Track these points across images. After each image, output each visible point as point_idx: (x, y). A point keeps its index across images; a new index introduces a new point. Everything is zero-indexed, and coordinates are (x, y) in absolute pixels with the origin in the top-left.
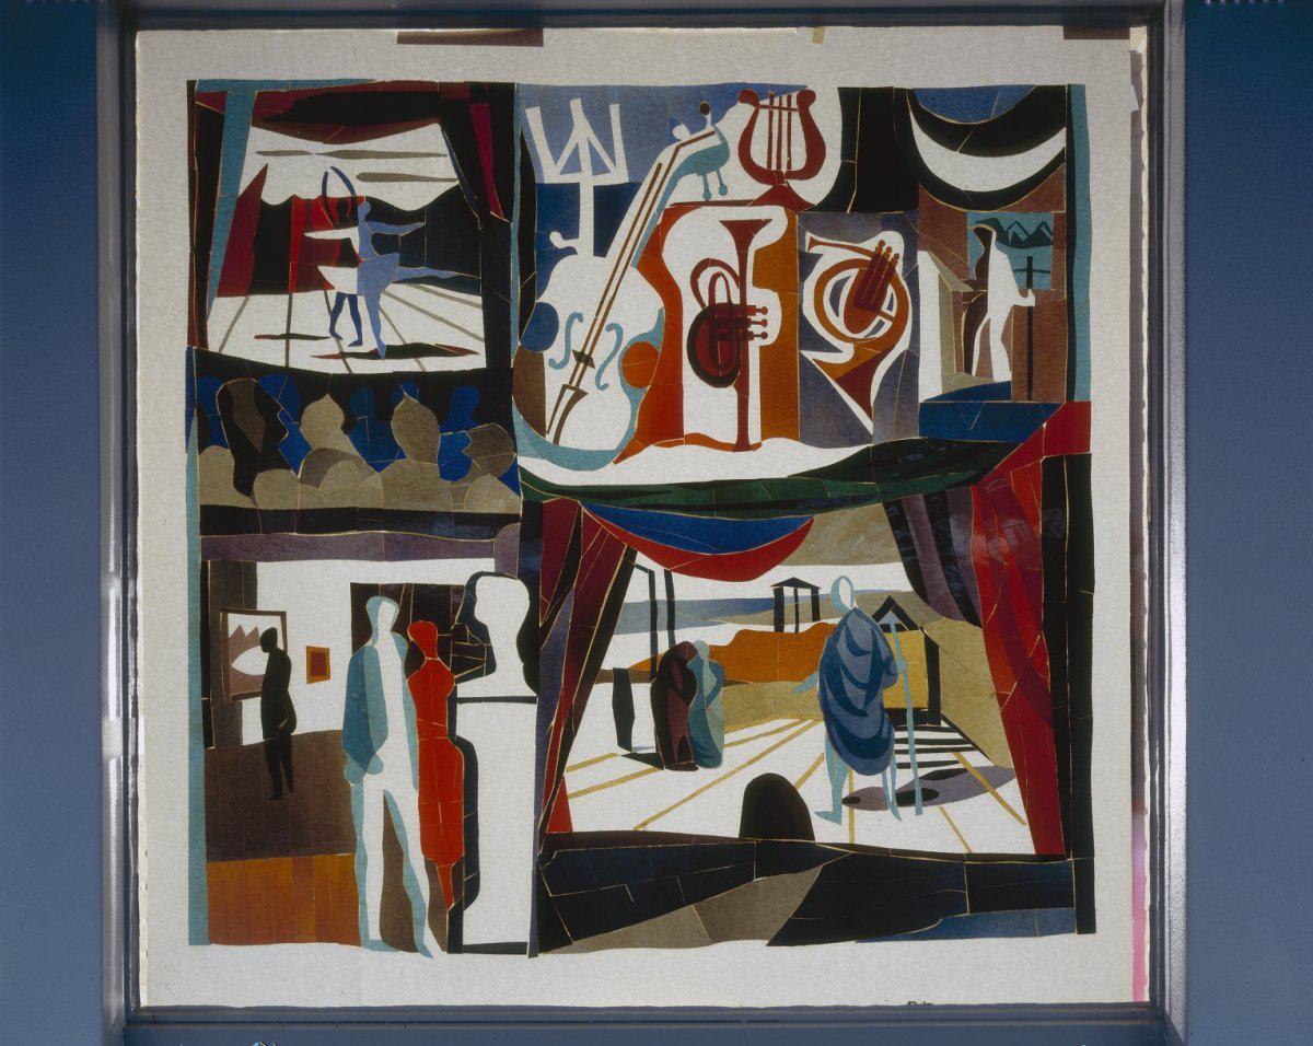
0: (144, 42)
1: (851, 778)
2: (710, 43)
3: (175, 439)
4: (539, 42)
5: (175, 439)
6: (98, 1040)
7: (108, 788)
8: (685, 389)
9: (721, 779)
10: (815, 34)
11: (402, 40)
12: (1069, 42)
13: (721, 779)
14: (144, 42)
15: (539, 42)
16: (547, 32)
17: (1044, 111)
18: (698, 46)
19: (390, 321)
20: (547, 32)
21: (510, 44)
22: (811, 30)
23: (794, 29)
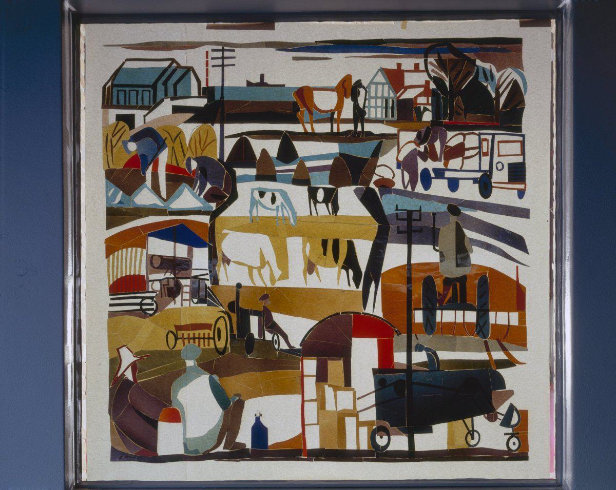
0: (83, 29)
1: (257, 207)
2: (354, 29)
3: (102, 214)
4: (273, 28)
5: (102, 214)
6: (63, 489)
7: (67, 382)
8: (298, 153)
9: (122, 128)
10: (403, 25)
11: (208, 28)
12: (522, 28)
13: (122, 128)
14: (83, 29)
15: (273, 28)
16: (276, 24)
17: (507, 50)
18: (348, 30)
19: (206, 140)
20: (276, 24)
21: (259, 29)
22: (401, 22)
23: (392, 22)
